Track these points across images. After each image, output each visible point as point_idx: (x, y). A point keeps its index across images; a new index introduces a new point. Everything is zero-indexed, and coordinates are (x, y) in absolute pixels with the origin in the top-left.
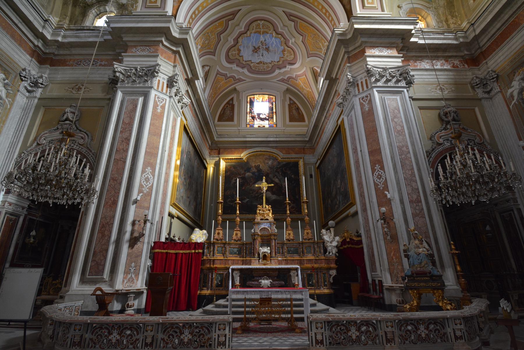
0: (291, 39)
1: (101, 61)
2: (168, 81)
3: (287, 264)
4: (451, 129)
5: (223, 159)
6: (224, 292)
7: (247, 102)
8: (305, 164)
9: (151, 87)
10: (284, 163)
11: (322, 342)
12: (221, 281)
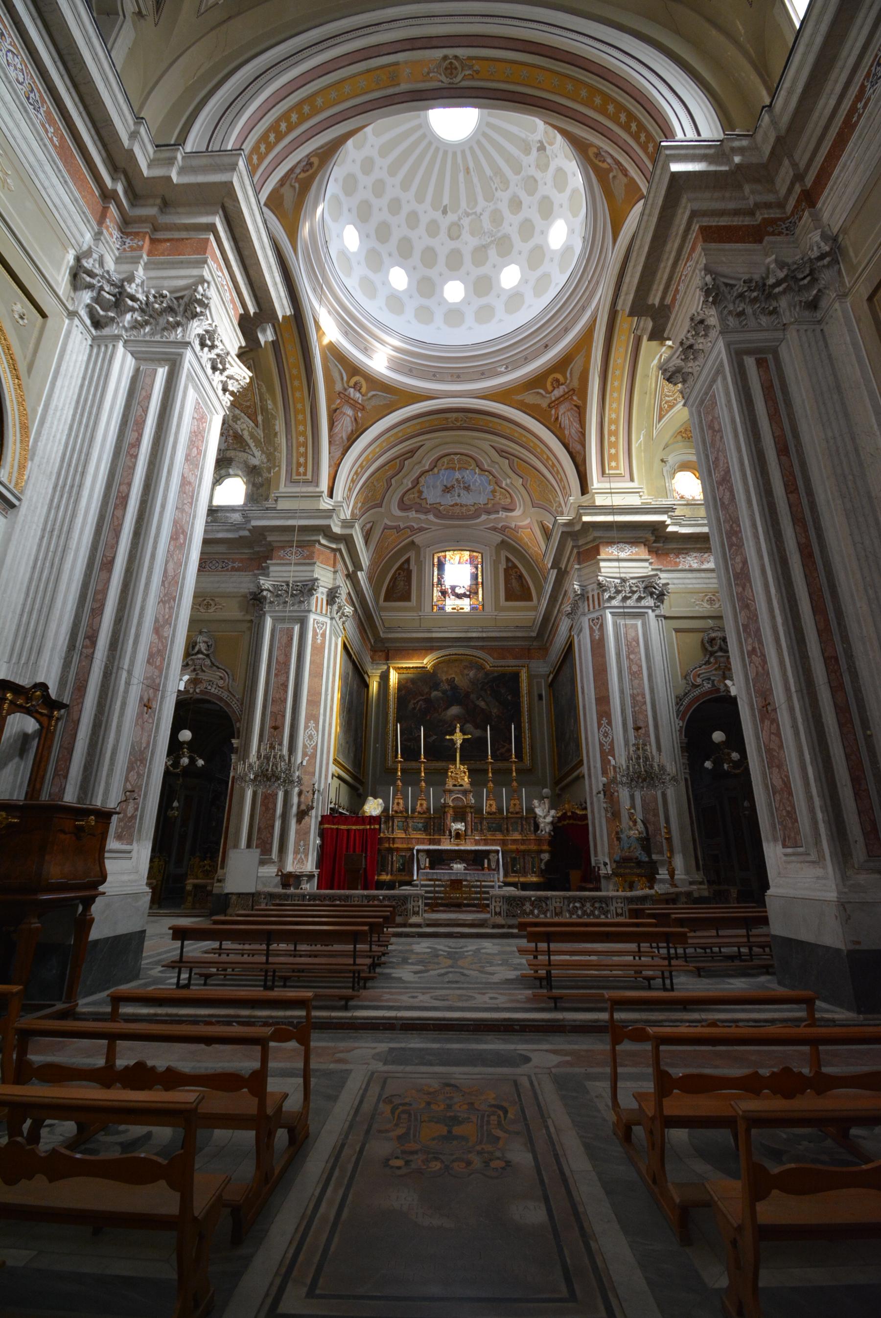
0: (505, 480)
1: (233, 562)
2: (328, 596)
3: (486, 844)
4: (716, 663)
5: (395, 669)
6: (407, 878)
7: (433, 565)
8: (530, 677)
9: (309, 611)
10: (496, 674)
11: (500, 914)
12: (403, 864)
